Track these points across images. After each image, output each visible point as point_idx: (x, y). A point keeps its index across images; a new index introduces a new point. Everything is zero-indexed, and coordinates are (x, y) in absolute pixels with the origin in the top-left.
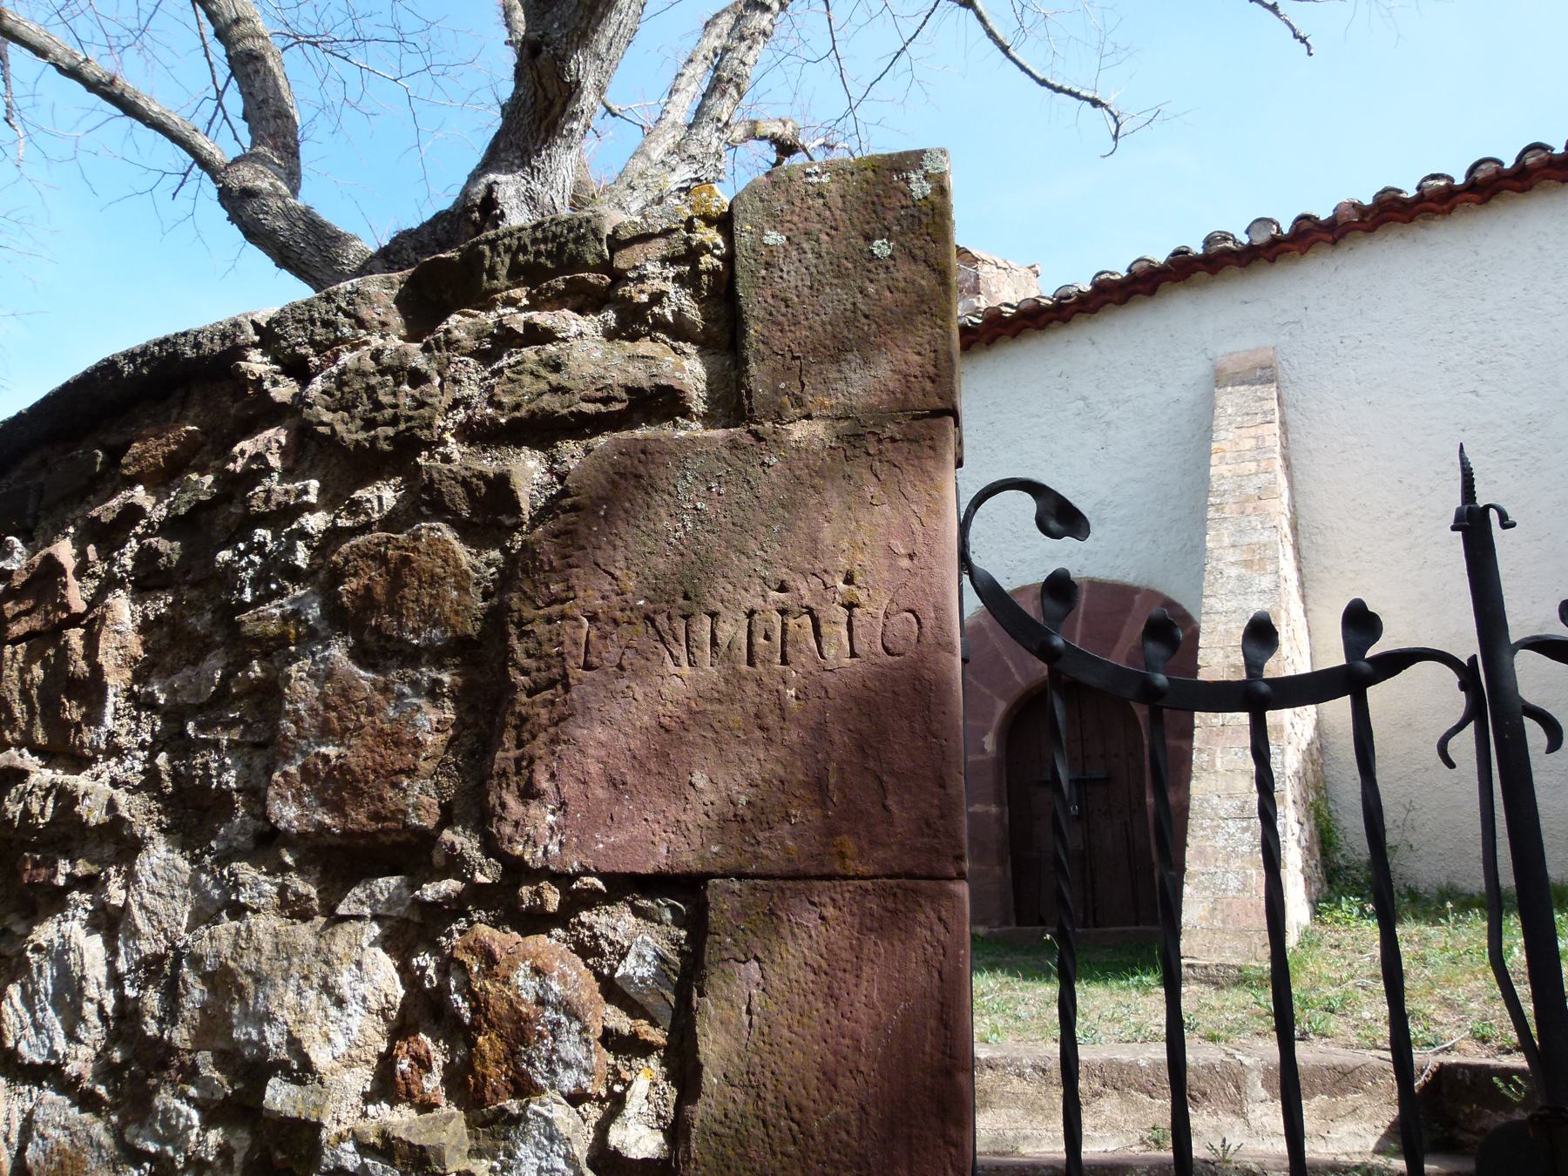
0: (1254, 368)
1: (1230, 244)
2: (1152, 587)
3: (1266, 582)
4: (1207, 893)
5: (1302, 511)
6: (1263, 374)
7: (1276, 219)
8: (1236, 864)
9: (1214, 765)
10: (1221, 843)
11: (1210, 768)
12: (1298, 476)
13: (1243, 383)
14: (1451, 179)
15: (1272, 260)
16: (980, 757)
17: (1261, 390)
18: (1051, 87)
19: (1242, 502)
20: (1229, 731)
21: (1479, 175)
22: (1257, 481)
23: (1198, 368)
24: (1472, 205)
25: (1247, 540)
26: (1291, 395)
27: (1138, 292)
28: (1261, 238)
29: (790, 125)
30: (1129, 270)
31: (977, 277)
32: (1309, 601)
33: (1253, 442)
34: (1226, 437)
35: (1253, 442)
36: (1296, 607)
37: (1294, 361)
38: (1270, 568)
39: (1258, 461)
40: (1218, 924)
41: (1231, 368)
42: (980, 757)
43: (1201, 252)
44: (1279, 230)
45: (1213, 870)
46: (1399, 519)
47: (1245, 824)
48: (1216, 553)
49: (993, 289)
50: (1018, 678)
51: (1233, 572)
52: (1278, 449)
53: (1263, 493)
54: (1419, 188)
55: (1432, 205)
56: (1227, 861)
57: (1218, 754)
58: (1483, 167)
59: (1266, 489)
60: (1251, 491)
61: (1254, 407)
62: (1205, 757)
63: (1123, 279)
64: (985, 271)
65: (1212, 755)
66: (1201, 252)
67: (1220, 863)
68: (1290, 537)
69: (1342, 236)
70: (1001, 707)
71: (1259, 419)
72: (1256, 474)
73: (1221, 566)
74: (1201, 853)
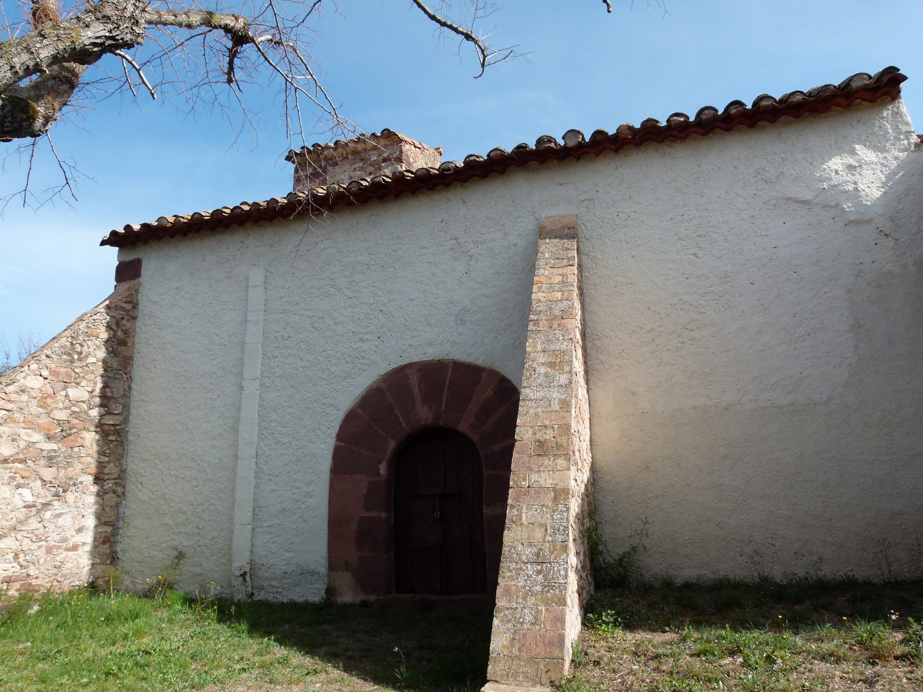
0: (563, 228)
1: (552, 145)
2: (493, 368)
3: (563, 379)
4: (509, 625)
5: (589, 323)
6: (568, 232)
7: (582, 131)
8: (531, 601)
9: (521, 519)
10: (522, 584)
11: (518, 521)
12: (588, 300)
13: (556, 237)
14: (687, 117)
15: (578, 159)
16: (377, 479)
17: (567, 243)
18: (438, 21)
19: (551, 320)
20: (532, 492)
21: (704, 117)
22: (561, 306)
23: (528, 225)
24: (698, 136)
25: (552, 347)
26: (585, 247)
27: (494, 171)
28: (572, 143)
29: (241, 20)
30: (488, 155)
31: (401, 152)
32: (591, 383)
33: (560, 278)
34: (544, 273)
35: (560, 278)
36: (582, 392)
37: (589, 225)
38: (567, 369)
39: (562, 291)
40: (515, 652)
41: (549, 226)
42: (377, 479)
43: (534, 148)
44: (583, 139)
45: (515, 606)
46: (648, 332)
47: (539, 568)
48: (532, 355)
49: (411, 160)
50: (404, 425)
51: (542, 370)
52: (575, 284)
53: (566, 314)
54: (668, 121)
55: (675, 133)
56: (525, 599)
57: (524, 510)
58: (706, 112)
59: (567, 312)
60: (557, 312)
61: (562, 254)
62: (515, 512)
63: (485, 161)
64: (406, 147)
65: (520, 510)
66: (534, 148)
67: (520, 600)
68: (580, 342)
69: (621, 147)
70: (392, 444)
71: (565, 262)
72: (561, 300)
73: (535, 365)
74: (507, 590)
